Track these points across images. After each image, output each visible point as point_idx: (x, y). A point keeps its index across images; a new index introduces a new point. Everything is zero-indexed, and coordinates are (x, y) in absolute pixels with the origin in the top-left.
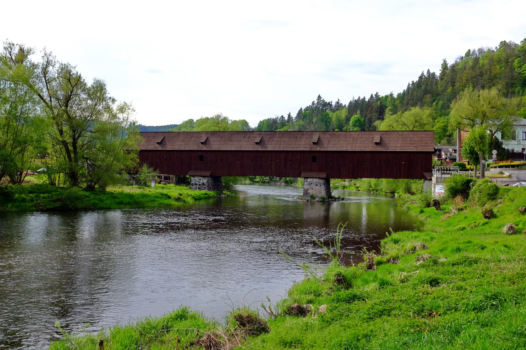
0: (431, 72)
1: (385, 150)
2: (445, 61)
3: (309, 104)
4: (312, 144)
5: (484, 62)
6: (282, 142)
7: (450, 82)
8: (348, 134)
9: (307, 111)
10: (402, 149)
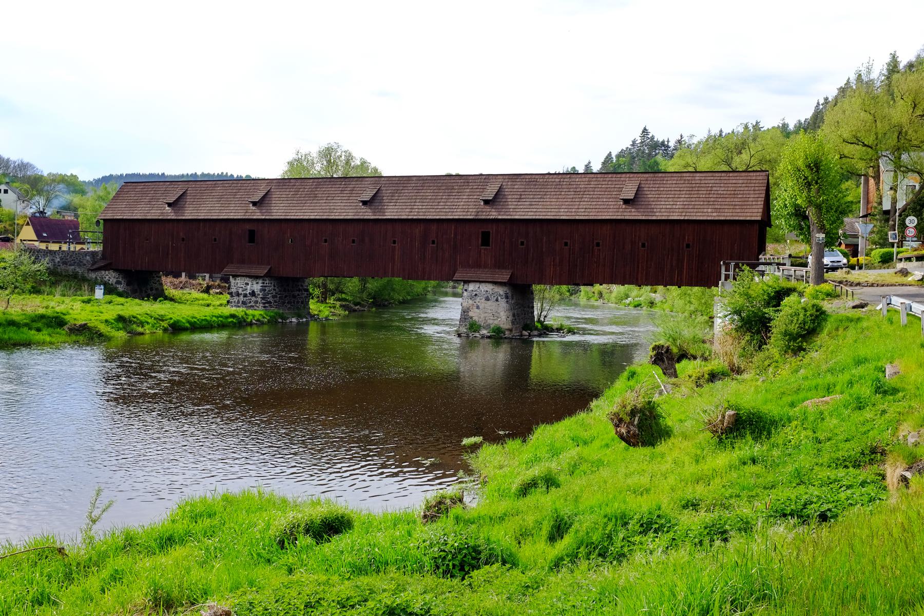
1: (644, 218)
2: (894, 57)
3: (626, 144)
4: (482, 203)
6: (418, 201)
8: (566, 180)
9: (621, 159)
10: (684, 214)
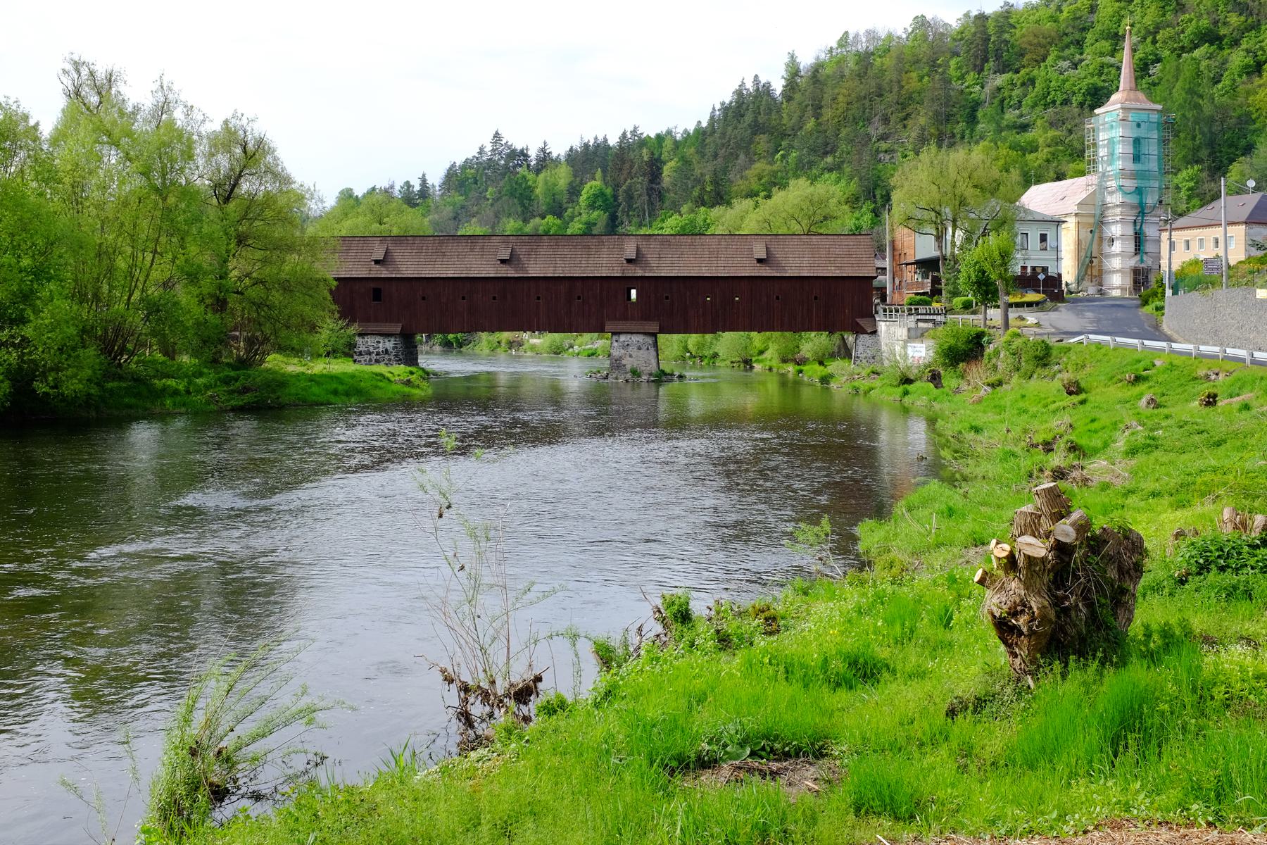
0: (763, 80)
3: (472, 152)
5: (883, 64)
7: (810, 107)
